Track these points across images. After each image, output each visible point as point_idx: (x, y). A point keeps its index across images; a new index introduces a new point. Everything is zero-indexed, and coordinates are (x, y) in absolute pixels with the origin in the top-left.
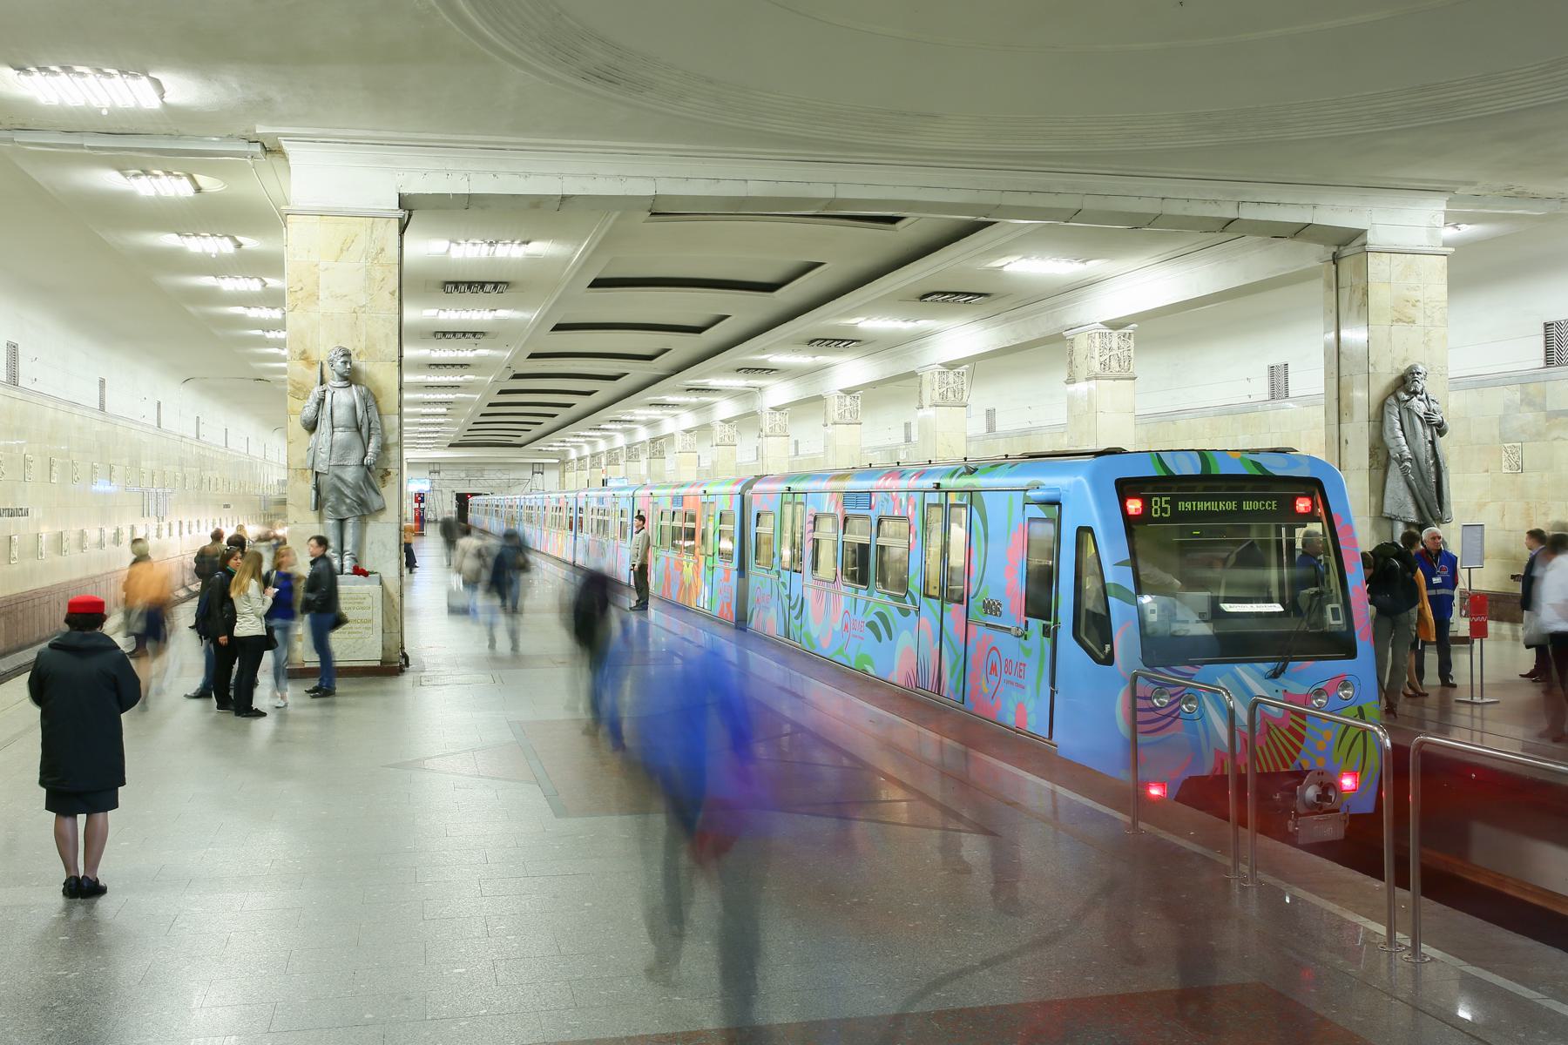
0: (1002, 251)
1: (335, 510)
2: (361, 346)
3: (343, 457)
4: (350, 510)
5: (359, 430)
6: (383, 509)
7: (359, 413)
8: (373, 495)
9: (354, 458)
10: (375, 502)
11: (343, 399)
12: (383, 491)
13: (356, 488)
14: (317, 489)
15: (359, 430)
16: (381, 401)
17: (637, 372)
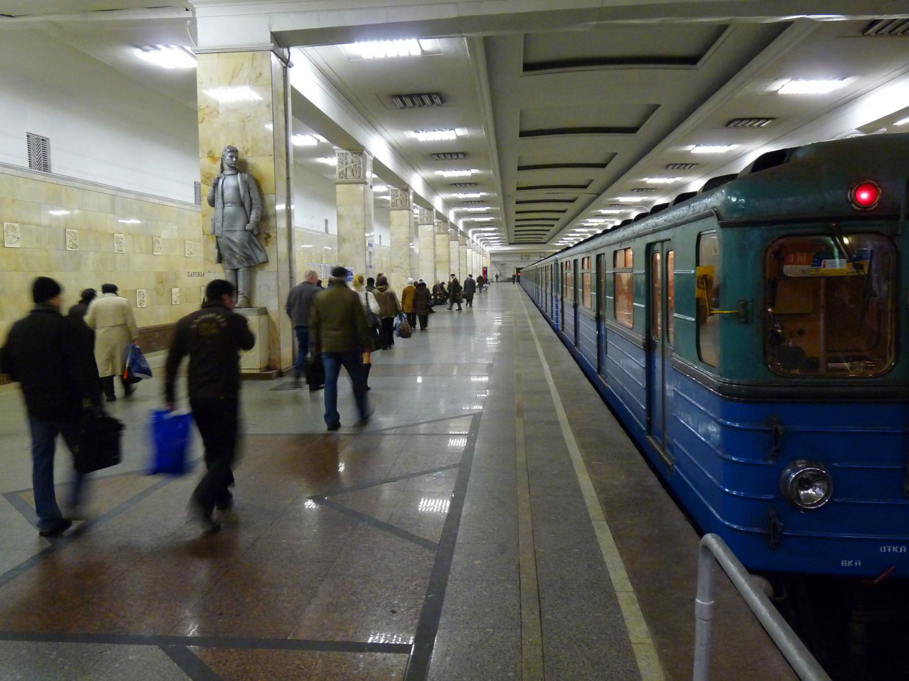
0: (778, 73)
1: (230, 263)
2: (248, 145)
3: (231, 225)
4: (240, 262)
5: (242, 205)
6: (266, 262)
7: (242, 192)
8: (258, 252)
9: (239, 225)
10: (261, 257)
11: (231, 182)
12: (266, 248)
14: (218, 247)
15: (242, 205)
16: (263, 186)
17: (582, 196)
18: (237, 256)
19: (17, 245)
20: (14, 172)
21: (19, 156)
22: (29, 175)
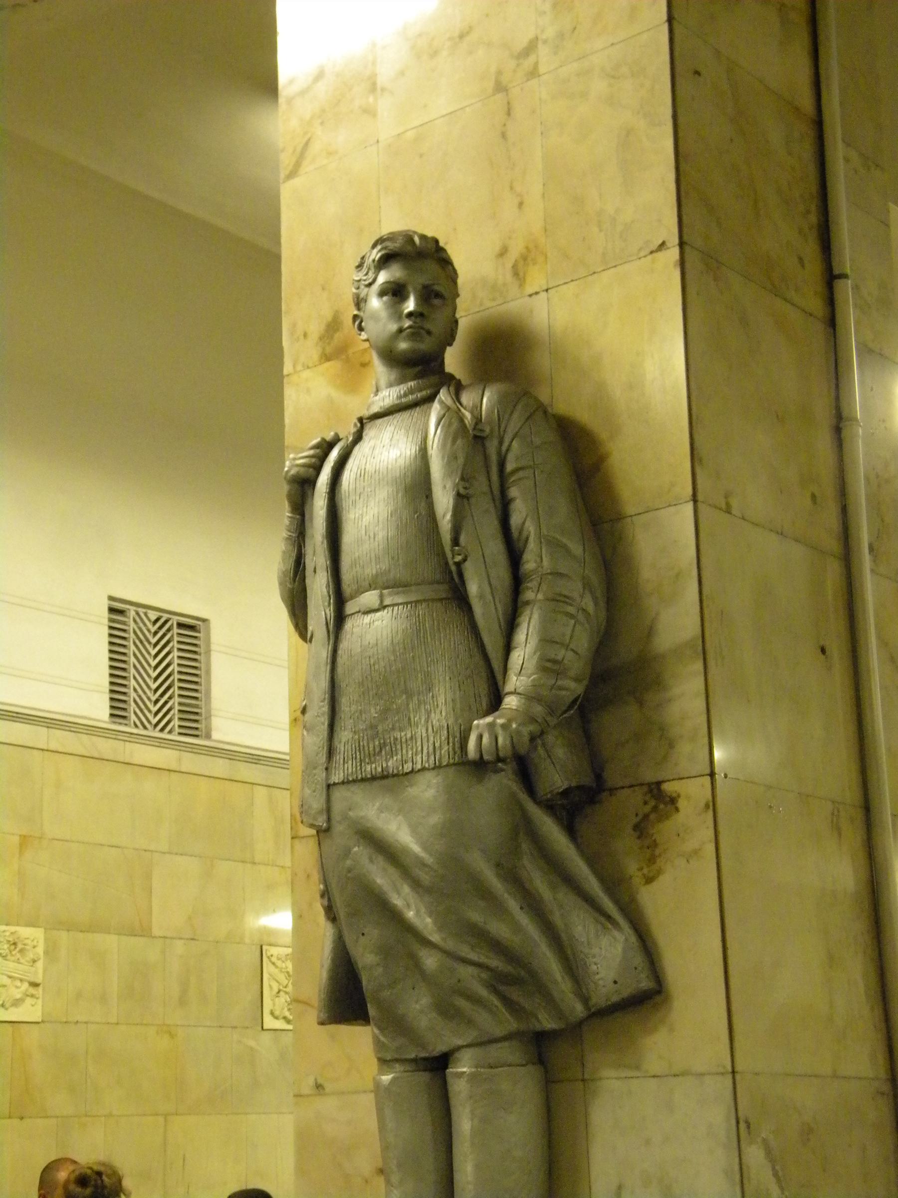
1: (395, 1024)
6: (647, 998)
10: (608, 957)
13: (450, 884)
18: (430, 961)
19: (30, 1011)
20: (58, 739)
21: (67, 673)
22: (106, 747)
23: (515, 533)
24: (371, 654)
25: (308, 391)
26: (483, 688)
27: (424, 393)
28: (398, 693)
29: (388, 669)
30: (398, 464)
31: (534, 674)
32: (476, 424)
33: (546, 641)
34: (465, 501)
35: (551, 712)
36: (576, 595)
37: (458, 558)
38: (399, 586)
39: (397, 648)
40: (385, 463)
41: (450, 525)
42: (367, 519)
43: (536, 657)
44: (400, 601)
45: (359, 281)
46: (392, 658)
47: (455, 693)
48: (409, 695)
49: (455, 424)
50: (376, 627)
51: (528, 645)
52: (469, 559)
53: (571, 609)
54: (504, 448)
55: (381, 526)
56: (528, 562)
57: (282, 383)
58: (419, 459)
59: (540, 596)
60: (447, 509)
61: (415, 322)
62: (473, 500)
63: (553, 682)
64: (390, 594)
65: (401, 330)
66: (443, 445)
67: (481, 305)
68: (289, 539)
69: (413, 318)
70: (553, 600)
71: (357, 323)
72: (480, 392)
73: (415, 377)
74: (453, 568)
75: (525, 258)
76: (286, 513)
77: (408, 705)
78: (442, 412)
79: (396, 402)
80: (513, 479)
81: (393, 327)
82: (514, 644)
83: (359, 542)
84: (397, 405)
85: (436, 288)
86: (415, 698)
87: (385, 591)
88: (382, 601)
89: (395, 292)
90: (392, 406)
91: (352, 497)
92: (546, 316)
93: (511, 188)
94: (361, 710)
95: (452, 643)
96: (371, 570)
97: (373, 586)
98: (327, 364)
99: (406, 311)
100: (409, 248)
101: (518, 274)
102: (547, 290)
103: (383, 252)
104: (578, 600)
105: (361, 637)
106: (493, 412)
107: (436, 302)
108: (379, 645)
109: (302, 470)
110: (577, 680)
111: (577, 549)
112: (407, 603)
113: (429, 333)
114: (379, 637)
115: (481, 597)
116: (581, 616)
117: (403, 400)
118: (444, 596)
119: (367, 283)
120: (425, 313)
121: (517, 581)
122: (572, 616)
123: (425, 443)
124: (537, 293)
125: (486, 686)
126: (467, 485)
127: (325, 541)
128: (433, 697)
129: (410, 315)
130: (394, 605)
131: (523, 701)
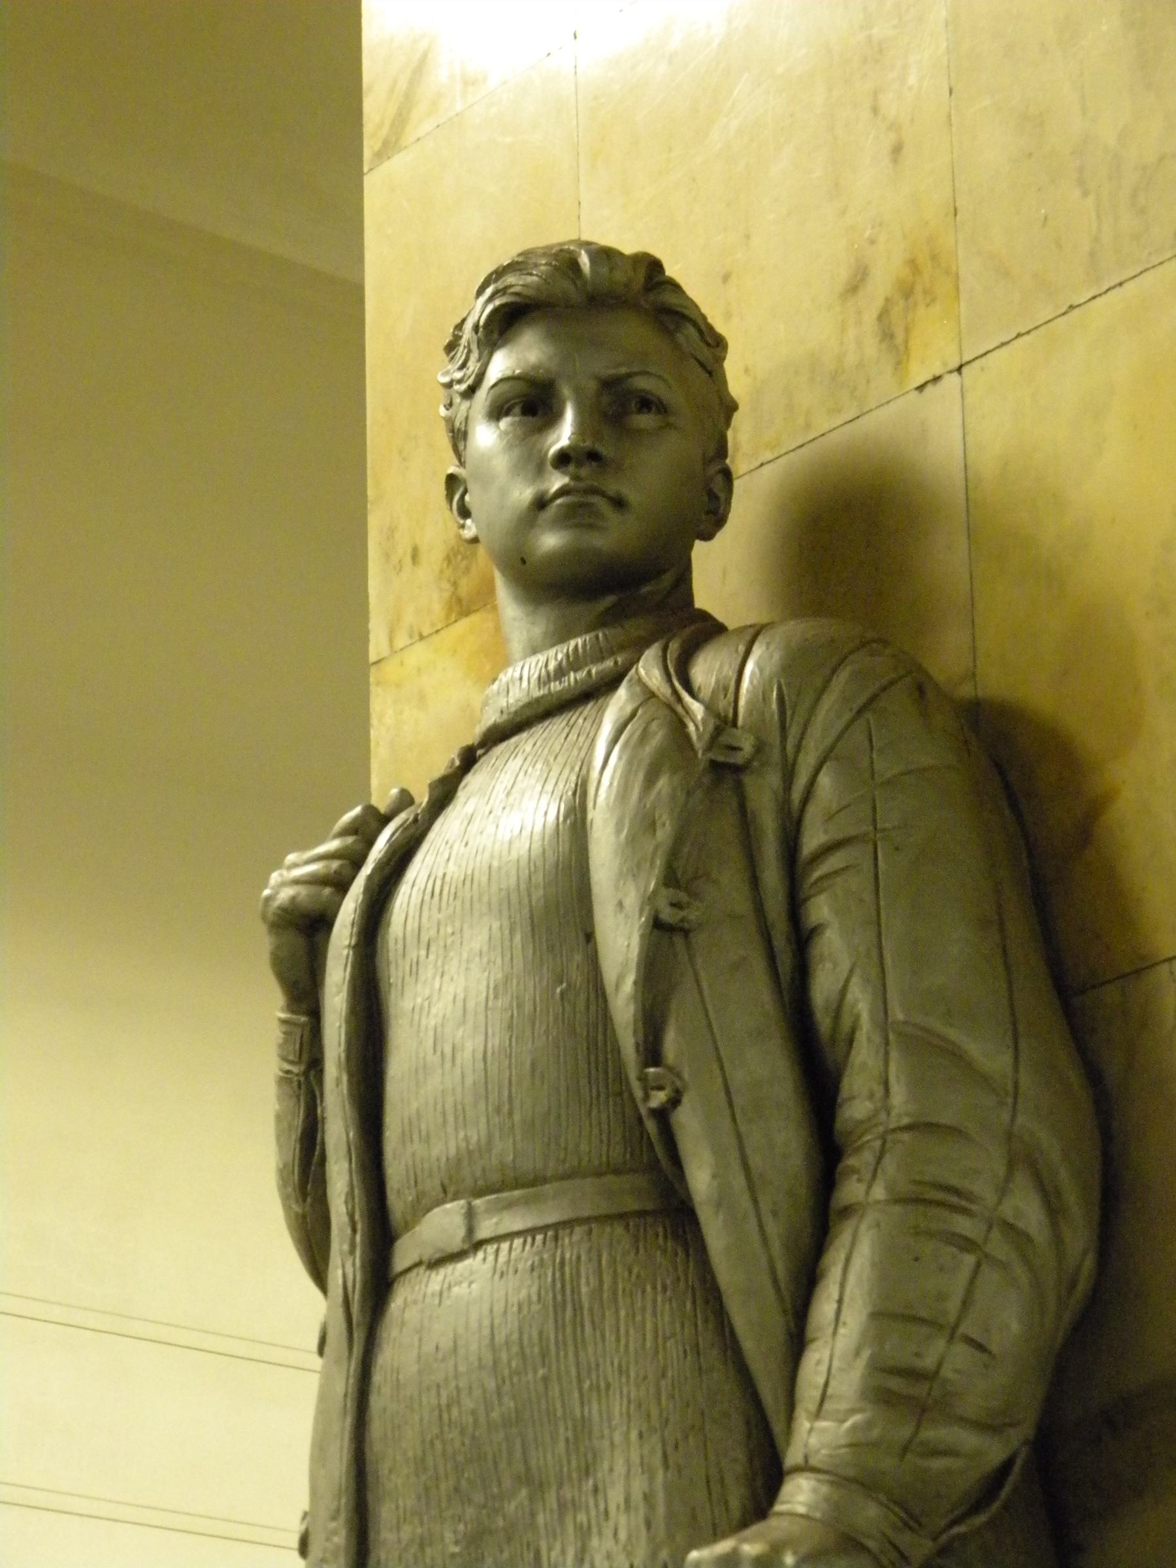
23: (824, 1022)
24: (439, 1377)
25: (422, 699)
26: (735, 1461)
27: (609, 663)
28: (507, 1483)
29: (482, 1420)
30: (514, 855)
31: (853, 1411)
32: (718, 731)
33: (889, 1316)
34: (678, 940)
35: (912, 1521)
36: (984, 1189)
37: (659, 1098)
38: (517, 1184)
39: (504, 1356)
40: (487, 855)
41: (632, 1008)
42: (442, 1008)
43: (861, 1363)
44: (518, 1226)
45: (449, 386)
46: (491, 1385)
47: (651, 1480)
48: (536, 1484)
49: (658, 736)
50: (468, 1295)
51: (842, 1331)
52: (685, 1100)
53: (964, 1225)
54: (796, 795)
55: (470, 1025)
56: (852, 1098)
57: (366, 676)
58: (565, 837)
59: (879, 1192)
60: (625, 965)
61: (575, 478)
62: (700, 939)
63: (905, 1432)
64: (493, 1209)
65: (541, 503)
66: (623, 794)
67: (808, 426)
68: (285, 1079)
69: (571, 468)
70: (918, 1201)
71: (457, 497)
72: (742, 648)
73: (602, 621)
74: (651, 1126)
75: (907, 292)
76: (271, 1005)
77: (533, 1515)
78: (629, 709)
79: (537, 693)
80: (816, 874)
81: (524, 494)
82: (810, 1332)
83: (421, 1071)
84: (538, 700)
85: (642, 383)
86: (551, 1498)
87: (478, 1202)
88: (470, 1230)
89: (531, 402)
90: (528, 705)
91: (412, 954)
92: (959, 436)
93: (875, 110)
94: (422, 1538)
95: (649, 1336)
96: (444, 1147)
97: (451, 1190)
98: (464, 624)
99: (553, 450)
100: (565, 286)
101: (893, 337)
102: (959, 369)
103: (497, 302)
104: (990, 1197)
105: (420, 1331)
106: (766, 699)
107: (644, 421)
108: (462, 1351)
109: (303, 891)
110: (990, 1426)
111: (988, 1053)
112: (532, 1232)
113: (619, 503)
114: (461, 1331)
115: (721, 1201)
116: (999, 1247)
117: (555, 687)
118: (632, 1205)
119: (463, 387)
120: (605, 450)
121: (828, 1151)
122: (966, 1244)
123: (584, 794)
124: (936, 379)
125: (740, 1454)
126: (683, 897)
127: (345, 1078)
128: (596, 1490)
129: (563, 459)
130: (498, 1239)
131: (825, 1489)
